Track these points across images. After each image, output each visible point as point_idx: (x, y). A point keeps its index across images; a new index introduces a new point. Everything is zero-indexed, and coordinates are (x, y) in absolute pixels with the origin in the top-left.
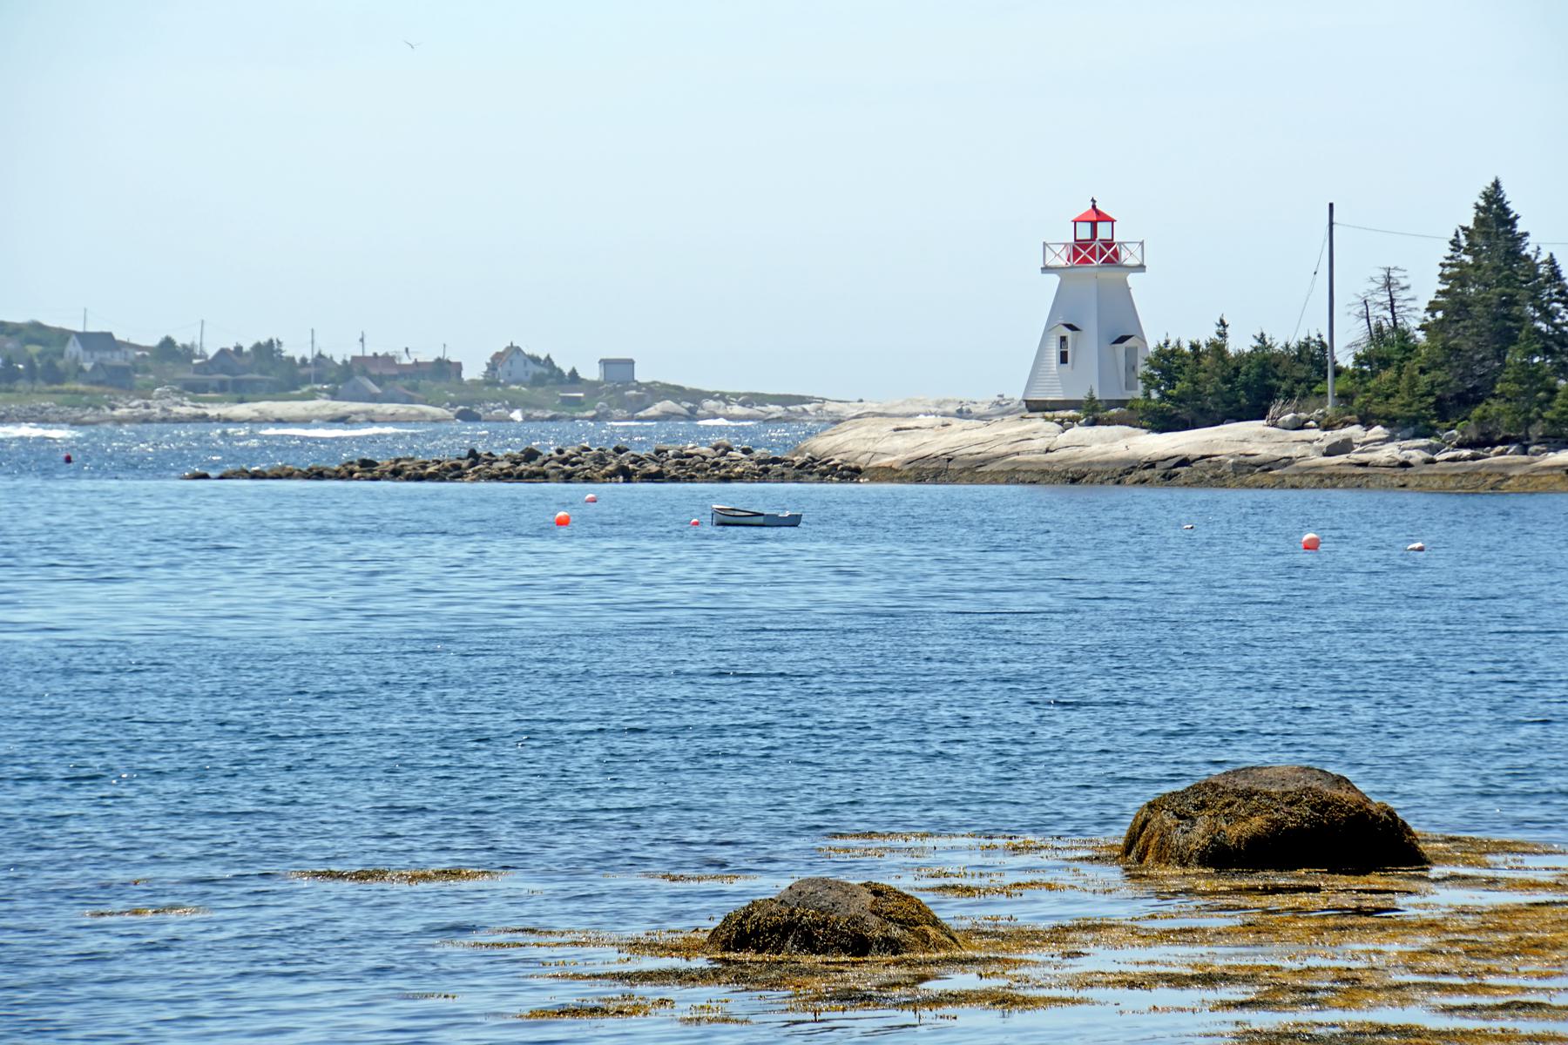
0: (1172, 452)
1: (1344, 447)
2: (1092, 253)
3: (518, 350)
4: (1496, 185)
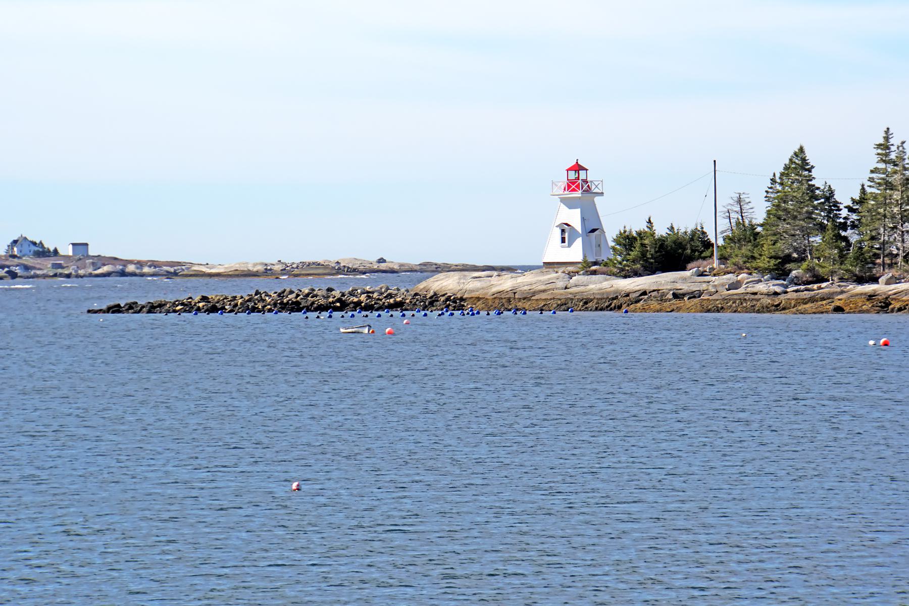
0: (637, 288)
1: (735, 285)
2: (578, 187)
3: (25, 238)
4: (801, 150)
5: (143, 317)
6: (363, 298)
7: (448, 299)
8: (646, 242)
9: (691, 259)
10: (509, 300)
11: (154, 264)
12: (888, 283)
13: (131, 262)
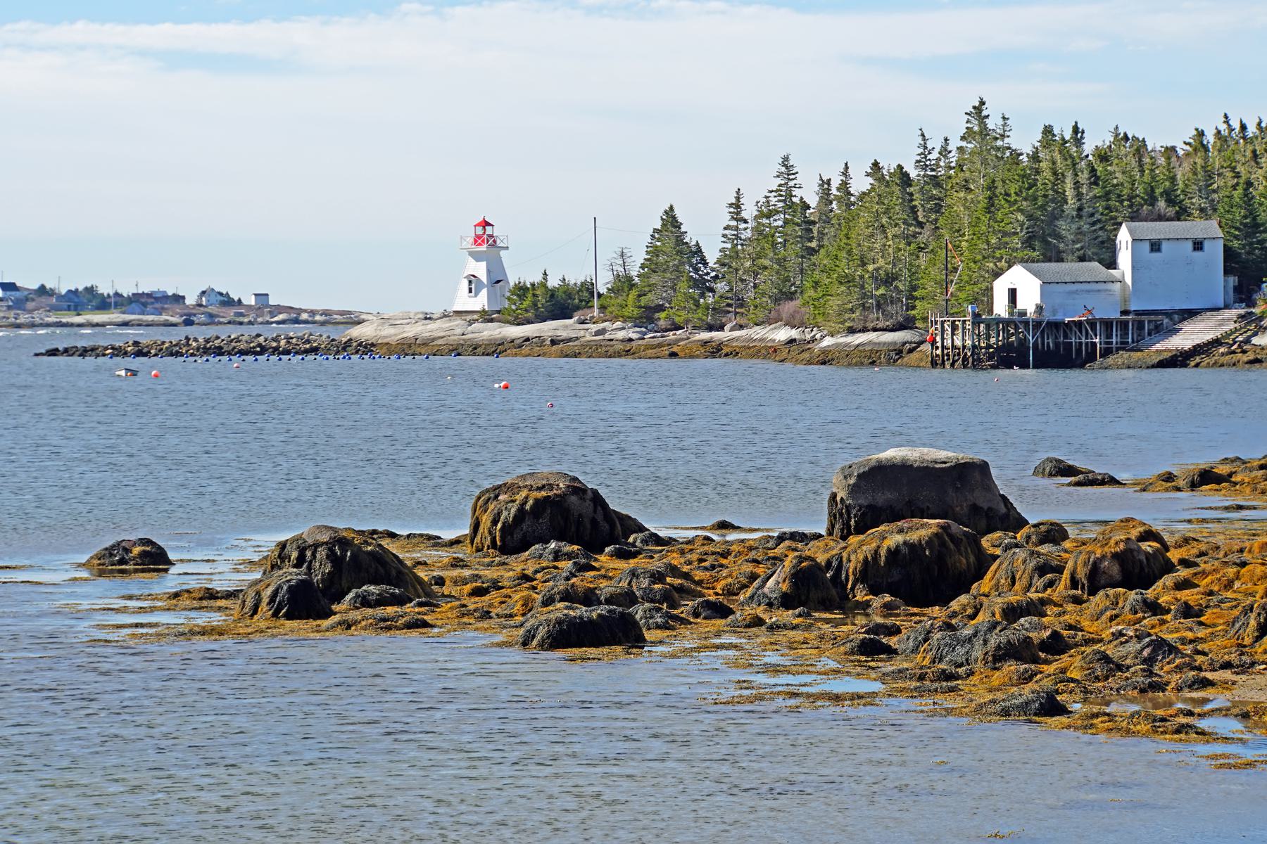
4: (671, 208)
5: (76, 359)
6: (283, 343)
7: (360, 345)
8: (538, 292)
9: (578, 308)
10: (410, 346)
11: (325, 313)
12: (731, 330)
13: (305, 311)
